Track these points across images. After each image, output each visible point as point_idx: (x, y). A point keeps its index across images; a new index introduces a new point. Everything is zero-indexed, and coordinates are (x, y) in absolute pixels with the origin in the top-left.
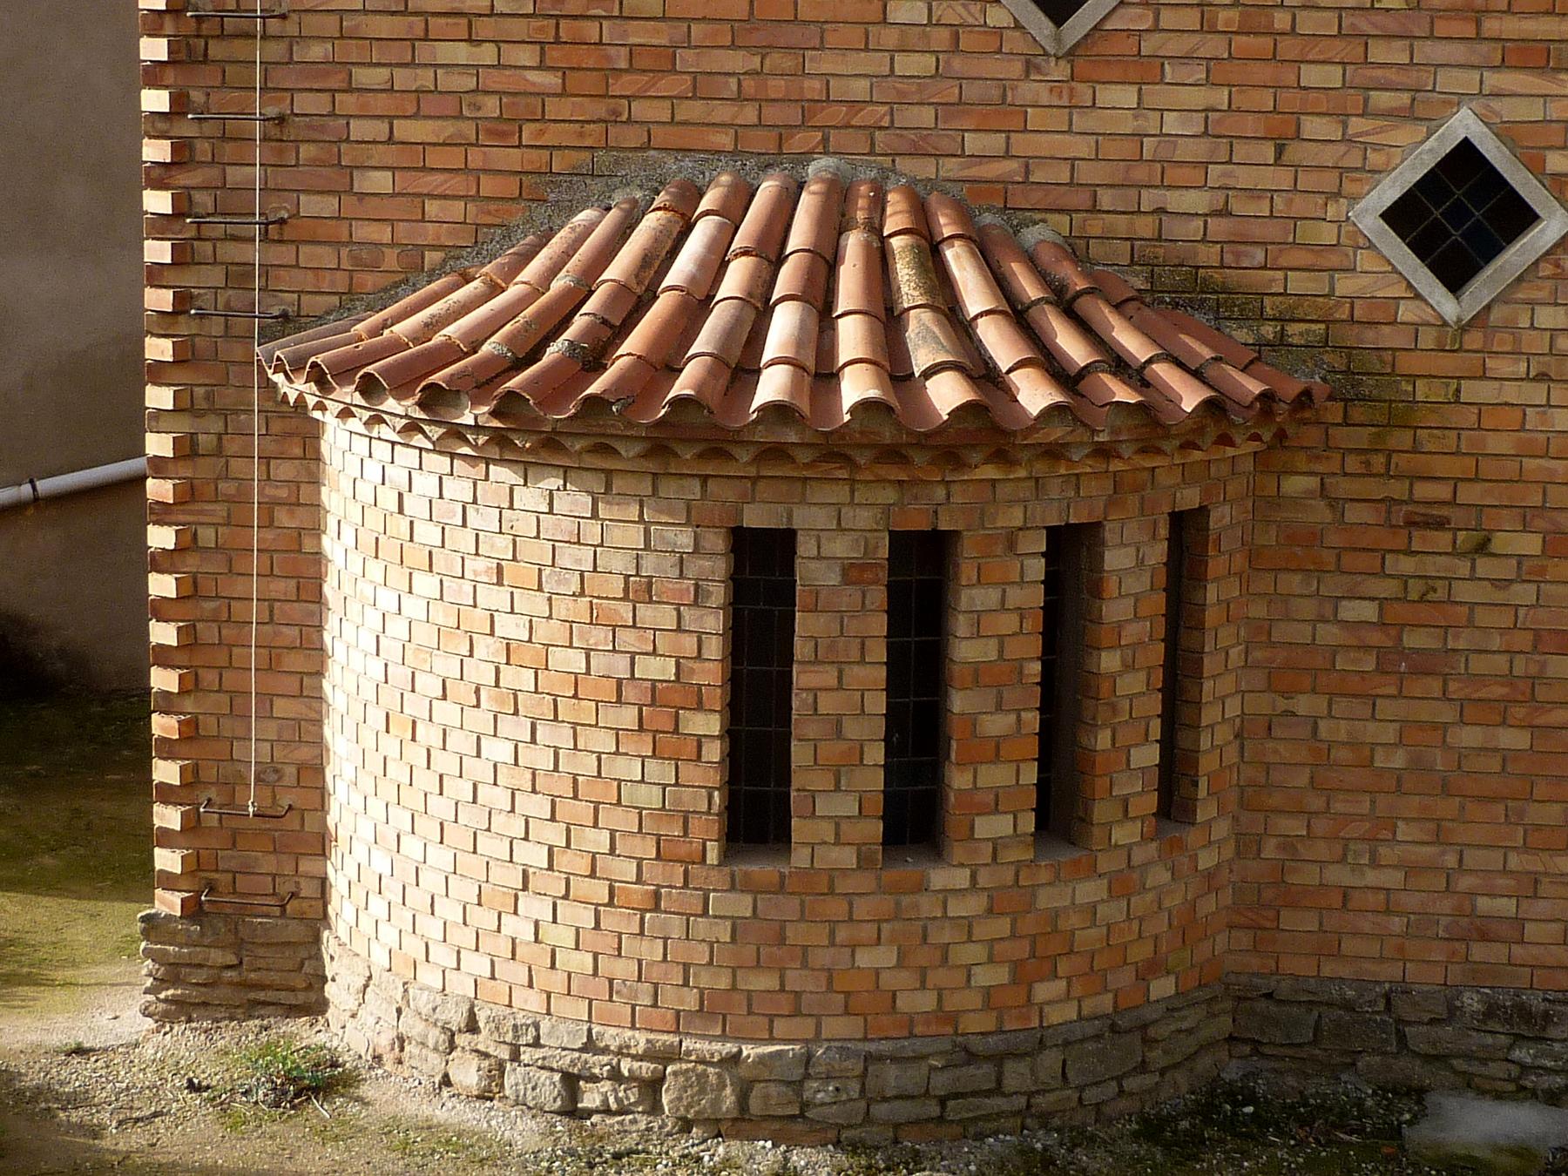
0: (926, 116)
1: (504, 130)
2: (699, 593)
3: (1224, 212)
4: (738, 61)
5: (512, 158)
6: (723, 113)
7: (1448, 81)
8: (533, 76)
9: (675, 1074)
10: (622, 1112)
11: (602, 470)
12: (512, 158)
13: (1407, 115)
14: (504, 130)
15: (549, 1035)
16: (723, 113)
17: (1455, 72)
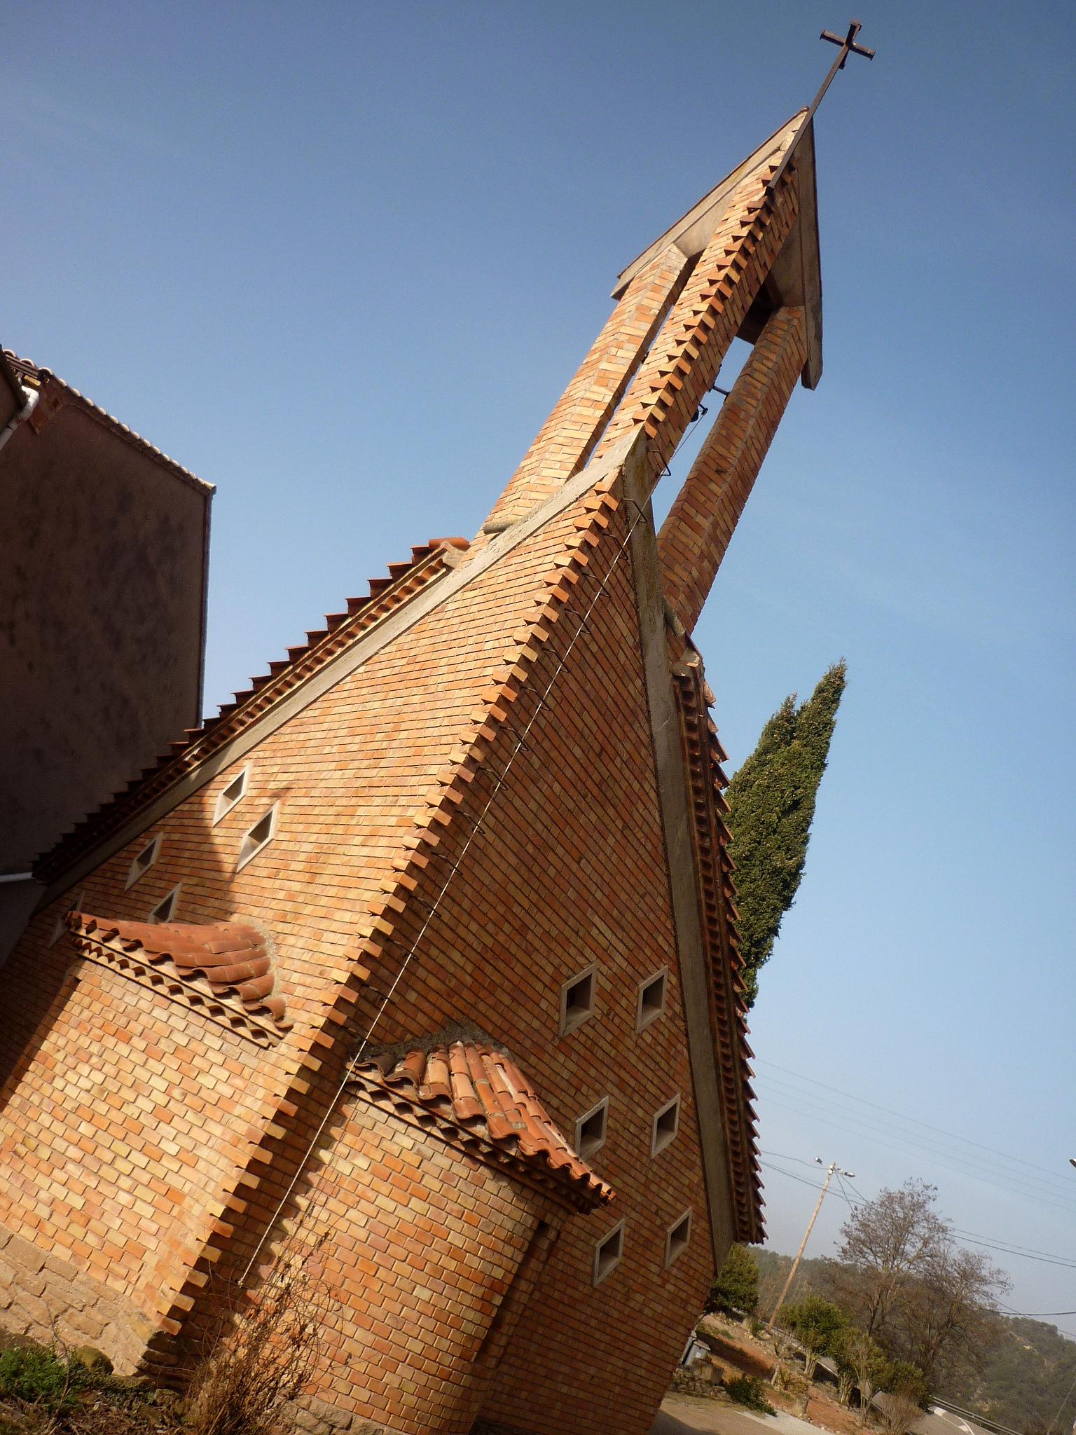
5: (446, 1007)
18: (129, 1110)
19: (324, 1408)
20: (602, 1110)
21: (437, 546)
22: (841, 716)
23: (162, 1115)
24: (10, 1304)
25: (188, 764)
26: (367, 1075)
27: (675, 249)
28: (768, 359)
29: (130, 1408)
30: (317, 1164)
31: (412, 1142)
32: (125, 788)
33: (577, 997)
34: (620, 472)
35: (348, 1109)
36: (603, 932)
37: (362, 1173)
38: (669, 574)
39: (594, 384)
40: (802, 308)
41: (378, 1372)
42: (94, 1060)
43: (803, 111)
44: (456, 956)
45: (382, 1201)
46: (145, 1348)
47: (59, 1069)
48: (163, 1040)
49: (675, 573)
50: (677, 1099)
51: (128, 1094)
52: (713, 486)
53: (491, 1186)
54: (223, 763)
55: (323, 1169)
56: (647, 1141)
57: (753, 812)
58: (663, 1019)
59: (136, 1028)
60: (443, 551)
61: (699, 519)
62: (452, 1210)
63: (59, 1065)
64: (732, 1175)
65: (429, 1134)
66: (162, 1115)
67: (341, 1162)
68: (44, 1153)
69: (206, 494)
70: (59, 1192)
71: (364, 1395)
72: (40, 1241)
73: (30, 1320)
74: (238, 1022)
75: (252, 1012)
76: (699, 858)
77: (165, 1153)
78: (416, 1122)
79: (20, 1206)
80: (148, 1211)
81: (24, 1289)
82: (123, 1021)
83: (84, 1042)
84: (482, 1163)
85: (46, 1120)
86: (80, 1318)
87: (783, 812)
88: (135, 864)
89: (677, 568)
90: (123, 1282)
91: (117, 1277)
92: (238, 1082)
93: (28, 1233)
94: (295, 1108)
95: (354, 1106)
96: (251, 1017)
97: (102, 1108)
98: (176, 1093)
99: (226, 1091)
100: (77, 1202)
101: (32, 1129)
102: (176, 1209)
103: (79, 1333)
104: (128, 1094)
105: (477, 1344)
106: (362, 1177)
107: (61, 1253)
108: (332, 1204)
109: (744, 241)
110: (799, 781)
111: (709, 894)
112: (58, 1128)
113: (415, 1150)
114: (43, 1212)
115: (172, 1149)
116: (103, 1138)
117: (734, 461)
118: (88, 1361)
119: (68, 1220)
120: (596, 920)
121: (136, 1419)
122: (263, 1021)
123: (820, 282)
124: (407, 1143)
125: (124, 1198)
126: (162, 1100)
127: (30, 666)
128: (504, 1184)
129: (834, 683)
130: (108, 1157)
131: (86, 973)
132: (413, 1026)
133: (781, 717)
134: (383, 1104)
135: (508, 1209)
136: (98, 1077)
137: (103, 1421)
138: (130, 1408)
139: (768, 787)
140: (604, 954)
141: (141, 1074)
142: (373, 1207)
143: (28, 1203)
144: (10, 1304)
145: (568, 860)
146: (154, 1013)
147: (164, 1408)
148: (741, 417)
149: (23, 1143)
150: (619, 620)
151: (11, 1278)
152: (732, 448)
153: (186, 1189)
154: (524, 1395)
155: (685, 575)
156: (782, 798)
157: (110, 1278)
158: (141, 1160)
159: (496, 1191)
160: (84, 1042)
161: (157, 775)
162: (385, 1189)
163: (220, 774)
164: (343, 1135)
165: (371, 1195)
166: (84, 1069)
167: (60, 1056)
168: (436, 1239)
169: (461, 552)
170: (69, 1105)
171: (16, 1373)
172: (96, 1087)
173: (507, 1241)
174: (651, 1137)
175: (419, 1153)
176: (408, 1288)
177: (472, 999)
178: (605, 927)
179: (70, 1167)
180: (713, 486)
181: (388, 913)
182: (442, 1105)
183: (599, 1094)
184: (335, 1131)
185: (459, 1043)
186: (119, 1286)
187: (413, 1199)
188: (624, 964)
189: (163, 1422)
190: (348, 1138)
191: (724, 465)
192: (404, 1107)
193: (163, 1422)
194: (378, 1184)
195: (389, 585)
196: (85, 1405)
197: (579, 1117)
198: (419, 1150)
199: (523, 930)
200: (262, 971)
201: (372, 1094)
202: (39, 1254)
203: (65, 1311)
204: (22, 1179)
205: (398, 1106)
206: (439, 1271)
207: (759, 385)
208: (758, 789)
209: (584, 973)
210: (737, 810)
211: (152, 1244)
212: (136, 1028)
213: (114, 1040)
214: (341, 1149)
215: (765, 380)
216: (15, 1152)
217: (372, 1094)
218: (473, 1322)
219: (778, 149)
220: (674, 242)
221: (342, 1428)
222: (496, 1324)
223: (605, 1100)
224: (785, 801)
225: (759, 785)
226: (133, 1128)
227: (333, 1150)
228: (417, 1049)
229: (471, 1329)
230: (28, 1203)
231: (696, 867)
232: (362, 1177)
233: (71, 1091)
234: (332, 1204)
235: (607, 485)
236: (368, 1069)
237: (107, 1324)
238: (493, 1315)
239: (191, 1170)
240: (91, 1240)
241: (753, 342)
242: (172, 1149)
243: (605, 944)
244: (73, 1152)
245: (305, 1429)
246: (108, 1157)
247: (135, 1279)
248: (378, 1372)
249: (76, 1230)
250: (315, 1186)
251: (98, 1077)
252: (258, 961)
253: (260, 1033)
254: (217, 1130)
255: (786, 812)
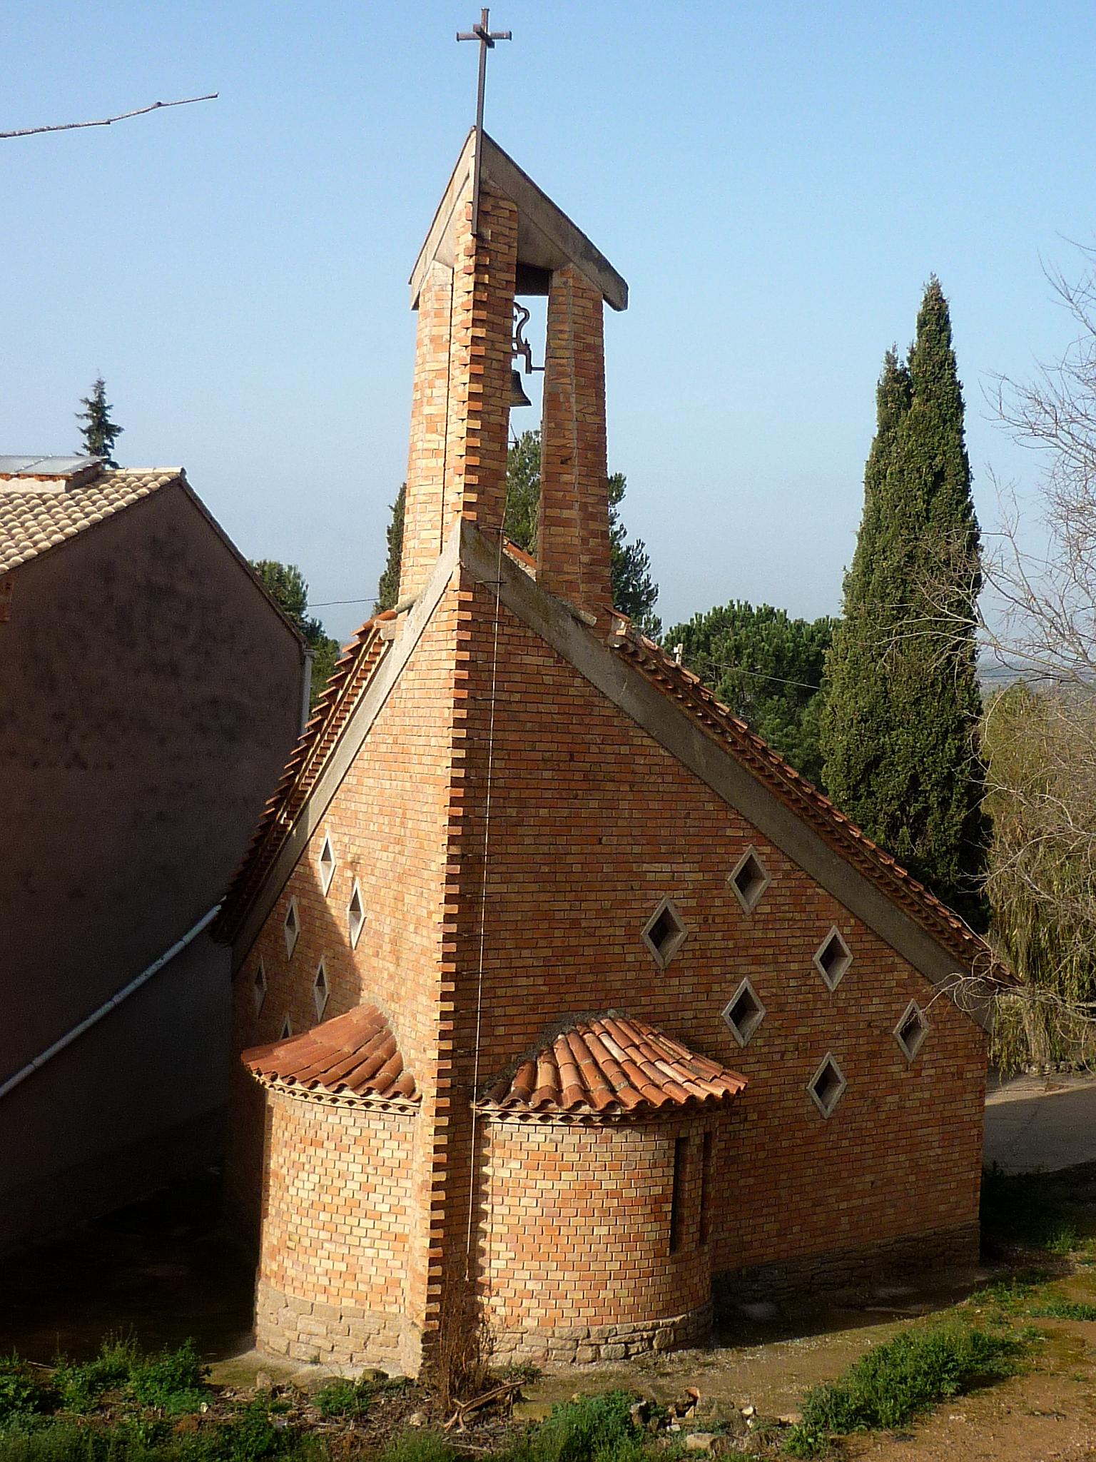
0: (632, 993)
1: (533, 1009)
2: (669, 1162)
3: (695, 1018)
4: (591, 978)
5: (535, 1018)
6: (588, 996)
7: (743, 970)
8: (542, 988)
9: (659, 1333)
10: (643, 1351)
11: (643, 1125)
12: (535, 1018)
13: (734, 982)
14: (533, 1009)
15: (621, 1331)
16: (588, 996)
17: (744, 967)
18: (344, 1193)
19: (566, 1332)
20: (746, 989)
21: (372, 626)
22: (960, 344)
23: (368, 1188)
24: (333, 1347)
25: (286, 826)
26: (487, 1107)
27: (438, 265)
28: (561, 332)
29: (404, 1394)
30: (486, 1178)
31: (544, 1136)
32: (247, 856)
33: (663, 930)
34: (461, 568)
35: (488, 1132)
36: (658, 871)
37: (518, 1172)
38: (561, 578)
39: (427, 432)
40: (571, 265)
41: (594, 1294)
42: (307, 1167)
43: (472, 131)
44: (523, 981)
45: (541, 1184)
46: (421, 1345)
47: (288, 1180)
48: (343, 1137)
49: (568, 573)
50: (834, 931)
51: (340, 1183)
52: (565, 478)
53: (618, 1138)
54: (309, 828)
55: (490, 1179)
56: (818, 982)
57: (896, 506)
58: (774, 884)
59: (322, 1135)
60: (378, 631)
61: (566, 514)
62: (596, 1168)
63: (287, 1178)
64: (950, 950)
65: (553, 1126)
66: (368, 1188)
67: (501, 1170)
68: (306, 1242)
69: (178, 483)
70: (328, 1264)
71: (591, 1312)
72: (331, 1299)
73: (350, 1352)
74: (385, 1107)
75: (390, 1098)
76: (729, 750)
77: (381, 1213)
78: (539, 1122)
79: (309, 1282)
80: (389, 1255)
81: (337, 1334)
82: (312, 1132)
83: (295, 1156)
84: (602, 1127)
85: (296, 1219)
86: (380, 1339)
87: (928, 493)
88: (287, 930)
89: (566, 568)
90: (395, 1305)
91: (390, 1304)
92: (406, 1146)
93: (321, 1298)
94: (445, 1155)
95: (491, 1128)
96: (391, 1101)
97: (327, 1199)
98: (370, 1170)
99: (402, 1155)
100: (342, 1267)
101: (291, 1228)
102: (407, 1246)
103: (384, 1348)
104: (340, 1183)
105: (666, 1243)
106: (520, 1174)
107: (348, 1303)
108: (507, 1200)
109: (474, 294)
110: (933, 449)
111: (761, 769)
112: (306, 1222)
113: (548, 1139)
114: (325, 1281)
115: (385, 1208)
116: (338, 1219)
117: (574, 444)
118: (370, 1377)
119: (342, 1280)
120: (646, 867)
121: (410, 1399)
122: (400, 1100)
123: (577, 229)
124: (541, 1138)
125: (370, 1252)
126: (363, 1178)
127: (111, 767)
128: (628, 1131)
129: (933, 309)
130: (347, 1230)
131: (270, 1101)
132: (514, 1048)
133: (886, 380)
134: (509, 1120)
135: (640, 1146)
136: (314, 1178)
137: (389, 1408)
138: (404, 1394)
139: (902, 471)
140: (673, 884)
141: (341, 1166)
142: (536, 1191)
143: (312, 1279)
144: (333, 1347)
145: (588, 849)
146: (329, 1120)
147: (426, 1385)
148: (561, 401)
149: (290, 1240)
150: (527, 660)
151: (325, 1331)
152: (567, 433)
153: (407, 1231)
154: (796, 1229)
155: (576, 569)
156: (921, 477)
157: (386, 1307)
158: (369, 1224)
159: (622, 1140)
160: (295, 1156)
161: (266, 840)
162: (539, 1175)
163: (312, 836)
164: (493, 1152)
165: (532, 1183)
166: (303, 1175)
167: (284, 1171)
168: (593, 1191)
169: (393, 621)
170: (305, 1204)
171: (327, 1403)
172: (317, 1186)
173: (654, 1166)
174: (820, 975)
175: (551, 1140)
176: (589, 1232)
177: (557, 998)
178: (660, 865)
179: (326, 1245)
180: (565, 478)
181: (444, 997)
182: (549, 1105)
183: (736, 982)
184: (486, 1151)
185: (560, 1037)
186: (394, 1309)
187: (563, 1173)
188: (700, 876)
189: (428, 1394)
190: (498, 1152)
191: (564, 453)
192: (525, 1117)
193: (428, 1394)
194: (532, 1174)
195: (354, 663)
196: (376, 1403)
197: (723, 1009)
198: (551, 1139)
199: (575, 923)
200: (392, 1051)
201: (499, 1117)
202: (334, 1309)
203: (369, 1337)
204: (301, 1265)
205: (520, 1118)
206: (606, 1212)
207: (564, 361)
208: (891, 478)
209: (653, 920)
210: (879, 512)
211: (402, 1274)
212: (322, 1135)
213: (312, 1149)
214: (497, 1162)
215: (567, 353)
216: (288, 1248)
217: (499, 1117)
218: (653, 1231)
219: (468, 177)
220: (434, 259)
221: (584, 1339)
222: (676, 1221)
223: (745, 982)
224: (925, 480)
225: (892, 474)
226: (352, 1206)
227: (490, 1165)
228: (524, 1063)
229: (653, 1236)
230: (312, 1279)
231: (732, 757)
232: (520, 1174)
233: (303, 1194)
234: (507, 1200)
235: (456, 582)
236: (487, 1103)
237: (398, 1336)
238: (669, 1218)
239: (403, 1217)
240: (362, 1287)
241: (547, 295)
242: (385, 1208)
243: (666, 876)
244: (324, 1235)
245: (557, 1349)
246: (347, 1230)
247: (402, 1301)
248: (594, 1294)
249: (350, 1285)
250: (490, 1193)
251: (314, 1178)
252: (386, 1045)
253: (403, 1108)
254: (408, 1184)
255: (932, 490)
